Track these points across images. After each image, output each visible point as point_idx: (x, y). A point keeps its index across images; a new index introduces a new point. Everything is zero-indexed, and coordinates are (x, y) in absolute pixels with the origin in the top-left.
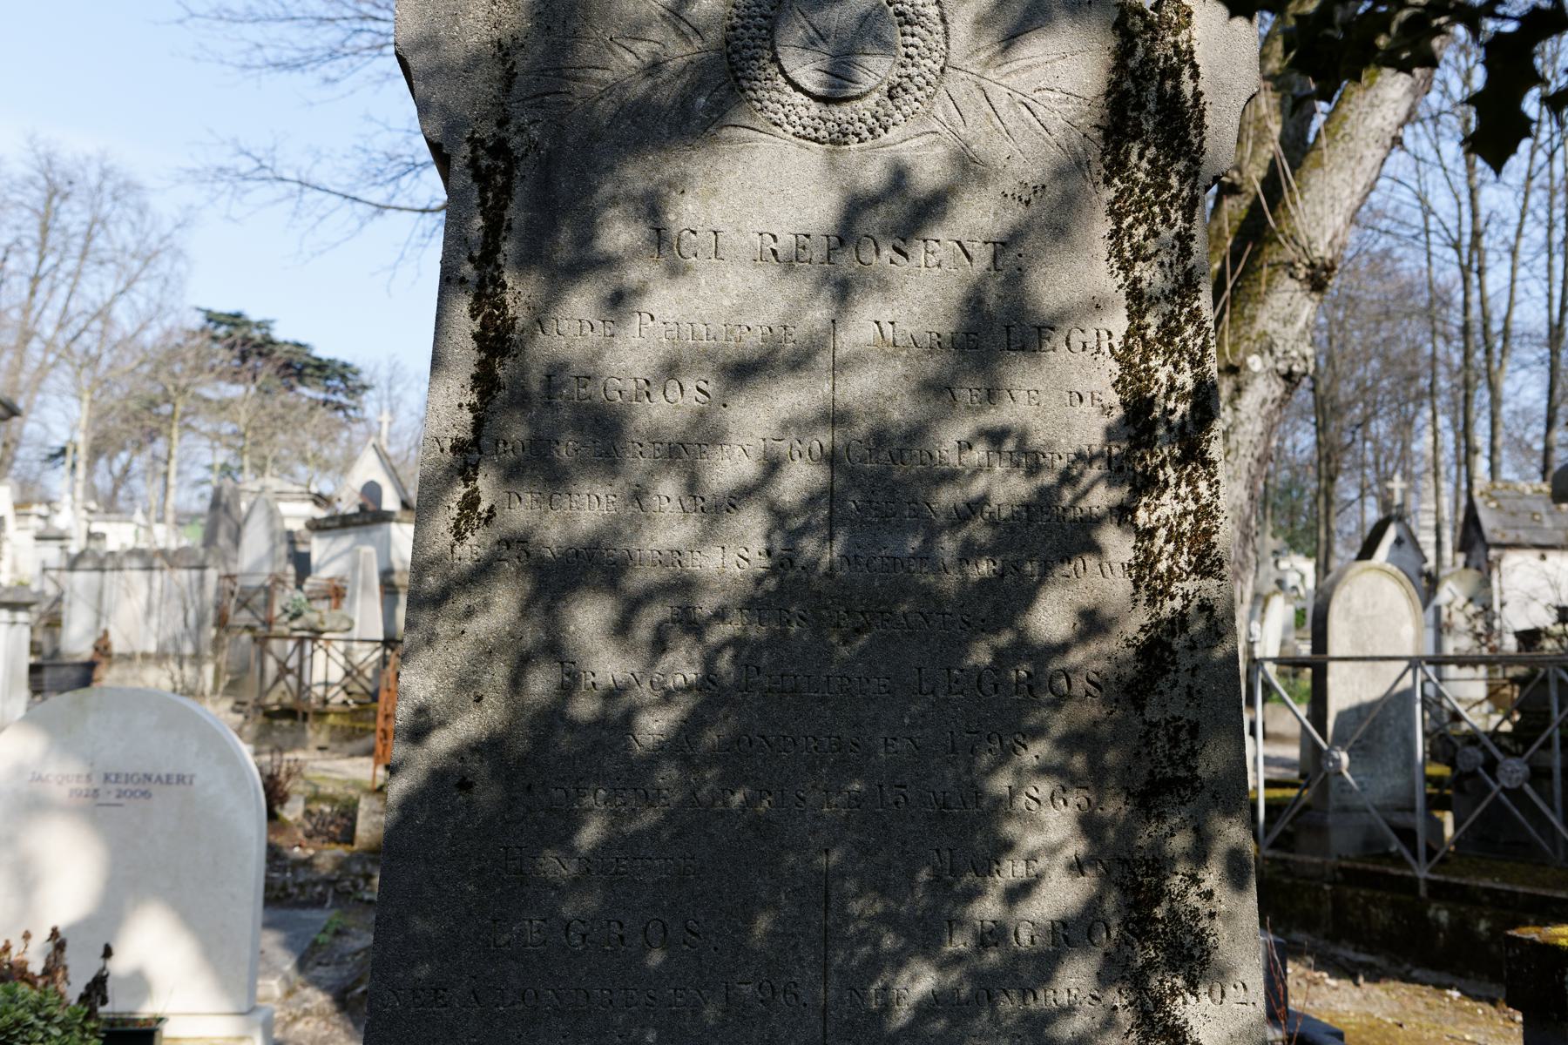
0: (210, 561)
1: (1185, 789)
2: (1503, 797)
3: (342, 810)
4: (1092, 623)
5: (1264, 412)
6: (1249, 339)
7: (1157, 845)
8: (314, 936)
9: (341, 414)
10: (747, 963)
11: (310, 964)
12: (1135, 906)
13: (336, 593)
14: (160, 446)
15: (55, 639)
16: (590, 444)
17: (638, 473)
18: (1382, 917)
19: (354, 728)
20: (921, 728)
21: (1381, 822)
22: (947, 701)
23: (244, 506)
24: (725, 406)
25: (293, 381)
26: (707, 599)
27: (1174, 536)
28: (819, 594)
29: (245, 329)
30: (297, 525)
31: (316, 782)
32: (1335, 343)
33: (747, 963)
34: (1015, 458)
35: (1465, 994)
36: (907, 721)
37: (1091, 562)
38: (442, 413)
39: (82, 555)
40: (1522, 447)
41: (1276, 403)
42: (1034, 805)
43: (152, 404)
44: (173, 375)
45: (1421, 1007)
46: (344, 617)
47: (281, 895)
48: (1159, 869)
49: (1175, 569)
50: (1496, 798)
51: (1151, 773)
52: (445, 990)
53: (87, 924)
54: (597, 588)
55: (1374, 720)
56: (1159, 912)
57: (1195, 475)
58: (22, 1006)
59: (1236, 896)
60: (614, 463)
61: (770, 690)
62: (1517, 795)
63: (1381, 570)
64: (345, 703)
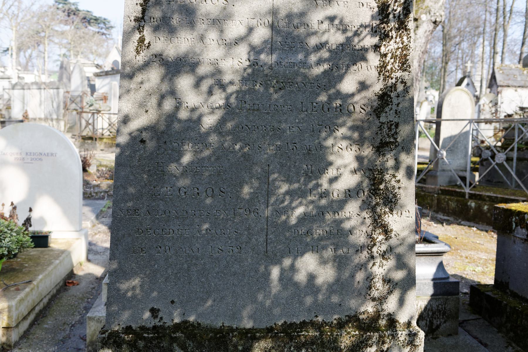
0: (61, 87)
1: (393, 145)
2: (496, 167)
3: (109, 169)
4: (363, 86)
5: (426, 35)
6: (422, 8)
7: (383, 164)
8: (101, 208)
9: (104, 37)
10: (241, 202)
11: (100, 217)
12: (374, 185)
13: (105, 98)
14: (41, 48)
15: (9, 113)
16: (184, 19)
17: (202, 30)
18: (453, 205)
19: (112, 143)
20: (302, 123)
21: (455, 174)
22: (311, 114)
23: (72, 68)
24: (233, 6)
25: (87, 24)
26: (227, 77)
27: (394, 57)
28: (267, 75)
29: (69, 5)
30: (90, 75)
31: (100, 161)
32: (452, 14)
33: (241, 202)
34: (338, 27)
35: (478, 229)
36: (297, 121)
37: (364, 64)
38: (130, 6)
39: (16, 84)
40: (513, 53)
41: (430, 32)
42: (340, 150)
43: (38, 33)
44: (44, 21)
45: (463, 233)
46: (108, 106)
47: (90, 196)
48: (382, 172)
49: (394, 68)
50: (494, 167)
51: (381, 140)
52: (138, 210)
53: (24, 202)
54: (187, 72)
55: (455, 141)
56: (382, 187)
57: (403, 34)
58: (2, 226)
59: (408, 182)
60: (193, 26)
61: (249, 109)
62: (501, 165)
63: (462, 90)
64: (109, 135)
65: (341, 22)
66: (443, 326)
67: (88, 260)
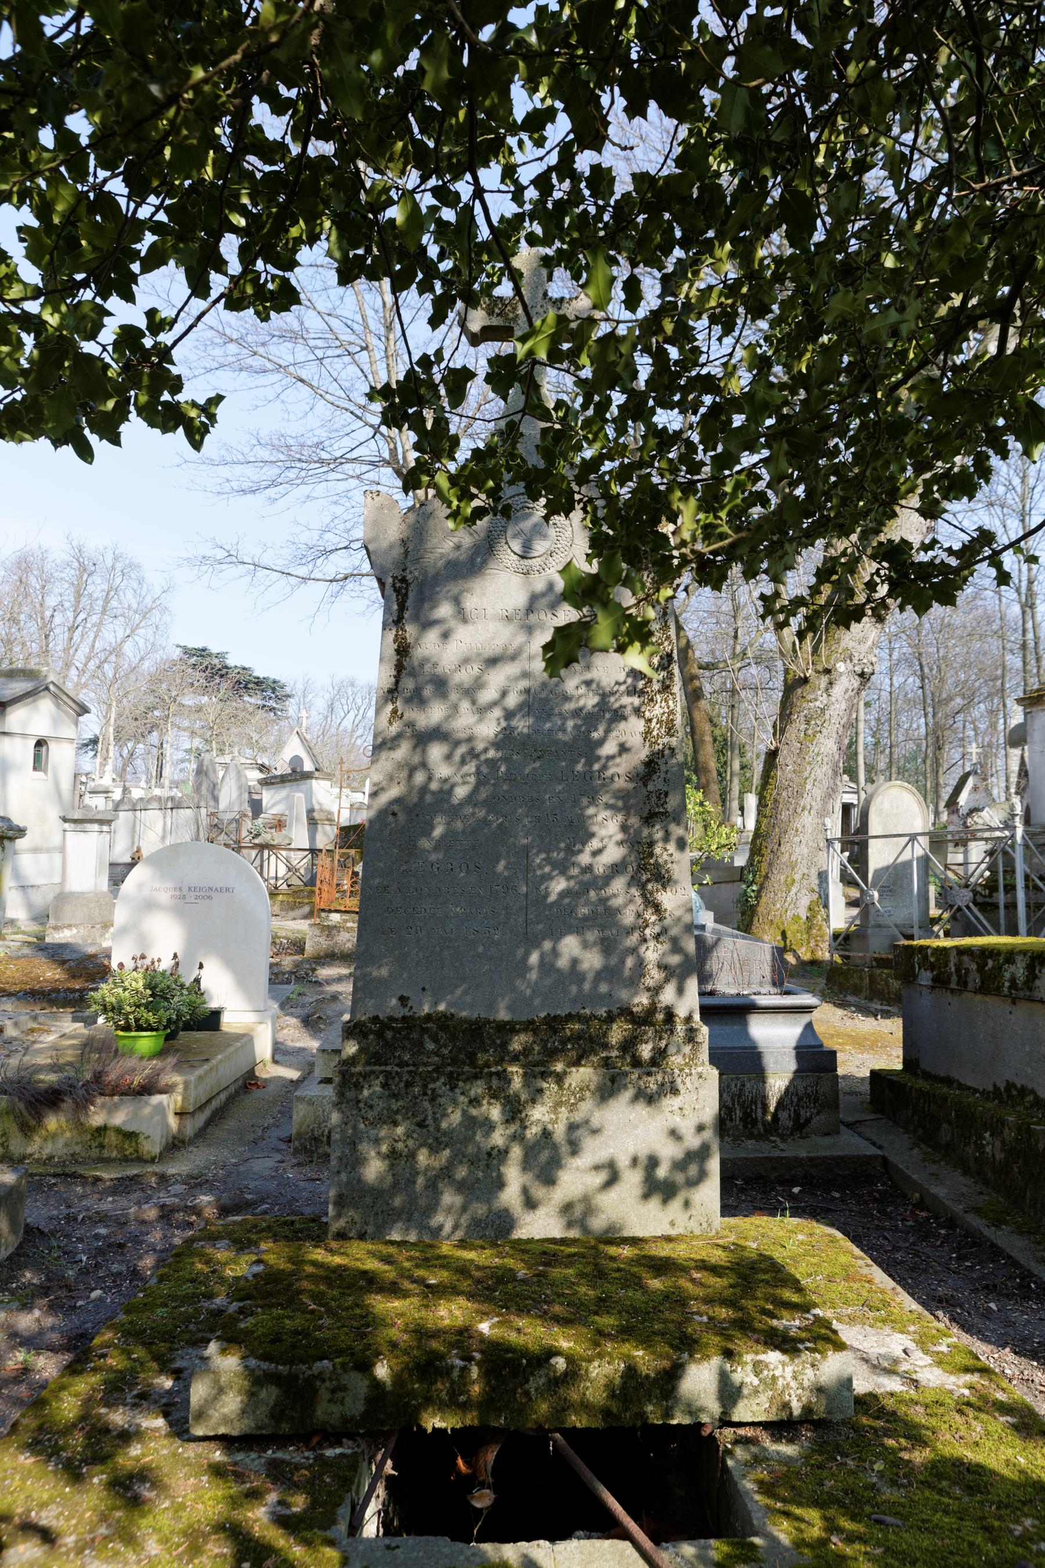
13: (279, 824)
39: (121, 801)
65: (598, 685)
66: (816, 1119)
67: (275, 1062)
